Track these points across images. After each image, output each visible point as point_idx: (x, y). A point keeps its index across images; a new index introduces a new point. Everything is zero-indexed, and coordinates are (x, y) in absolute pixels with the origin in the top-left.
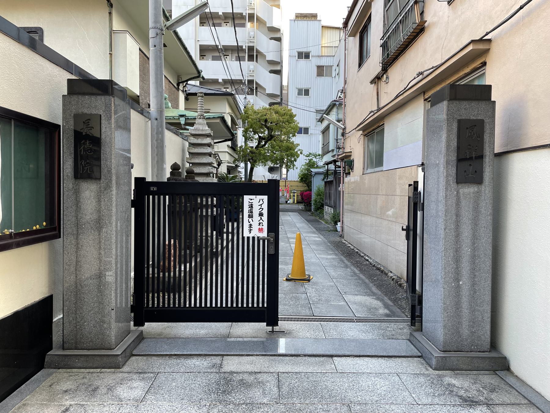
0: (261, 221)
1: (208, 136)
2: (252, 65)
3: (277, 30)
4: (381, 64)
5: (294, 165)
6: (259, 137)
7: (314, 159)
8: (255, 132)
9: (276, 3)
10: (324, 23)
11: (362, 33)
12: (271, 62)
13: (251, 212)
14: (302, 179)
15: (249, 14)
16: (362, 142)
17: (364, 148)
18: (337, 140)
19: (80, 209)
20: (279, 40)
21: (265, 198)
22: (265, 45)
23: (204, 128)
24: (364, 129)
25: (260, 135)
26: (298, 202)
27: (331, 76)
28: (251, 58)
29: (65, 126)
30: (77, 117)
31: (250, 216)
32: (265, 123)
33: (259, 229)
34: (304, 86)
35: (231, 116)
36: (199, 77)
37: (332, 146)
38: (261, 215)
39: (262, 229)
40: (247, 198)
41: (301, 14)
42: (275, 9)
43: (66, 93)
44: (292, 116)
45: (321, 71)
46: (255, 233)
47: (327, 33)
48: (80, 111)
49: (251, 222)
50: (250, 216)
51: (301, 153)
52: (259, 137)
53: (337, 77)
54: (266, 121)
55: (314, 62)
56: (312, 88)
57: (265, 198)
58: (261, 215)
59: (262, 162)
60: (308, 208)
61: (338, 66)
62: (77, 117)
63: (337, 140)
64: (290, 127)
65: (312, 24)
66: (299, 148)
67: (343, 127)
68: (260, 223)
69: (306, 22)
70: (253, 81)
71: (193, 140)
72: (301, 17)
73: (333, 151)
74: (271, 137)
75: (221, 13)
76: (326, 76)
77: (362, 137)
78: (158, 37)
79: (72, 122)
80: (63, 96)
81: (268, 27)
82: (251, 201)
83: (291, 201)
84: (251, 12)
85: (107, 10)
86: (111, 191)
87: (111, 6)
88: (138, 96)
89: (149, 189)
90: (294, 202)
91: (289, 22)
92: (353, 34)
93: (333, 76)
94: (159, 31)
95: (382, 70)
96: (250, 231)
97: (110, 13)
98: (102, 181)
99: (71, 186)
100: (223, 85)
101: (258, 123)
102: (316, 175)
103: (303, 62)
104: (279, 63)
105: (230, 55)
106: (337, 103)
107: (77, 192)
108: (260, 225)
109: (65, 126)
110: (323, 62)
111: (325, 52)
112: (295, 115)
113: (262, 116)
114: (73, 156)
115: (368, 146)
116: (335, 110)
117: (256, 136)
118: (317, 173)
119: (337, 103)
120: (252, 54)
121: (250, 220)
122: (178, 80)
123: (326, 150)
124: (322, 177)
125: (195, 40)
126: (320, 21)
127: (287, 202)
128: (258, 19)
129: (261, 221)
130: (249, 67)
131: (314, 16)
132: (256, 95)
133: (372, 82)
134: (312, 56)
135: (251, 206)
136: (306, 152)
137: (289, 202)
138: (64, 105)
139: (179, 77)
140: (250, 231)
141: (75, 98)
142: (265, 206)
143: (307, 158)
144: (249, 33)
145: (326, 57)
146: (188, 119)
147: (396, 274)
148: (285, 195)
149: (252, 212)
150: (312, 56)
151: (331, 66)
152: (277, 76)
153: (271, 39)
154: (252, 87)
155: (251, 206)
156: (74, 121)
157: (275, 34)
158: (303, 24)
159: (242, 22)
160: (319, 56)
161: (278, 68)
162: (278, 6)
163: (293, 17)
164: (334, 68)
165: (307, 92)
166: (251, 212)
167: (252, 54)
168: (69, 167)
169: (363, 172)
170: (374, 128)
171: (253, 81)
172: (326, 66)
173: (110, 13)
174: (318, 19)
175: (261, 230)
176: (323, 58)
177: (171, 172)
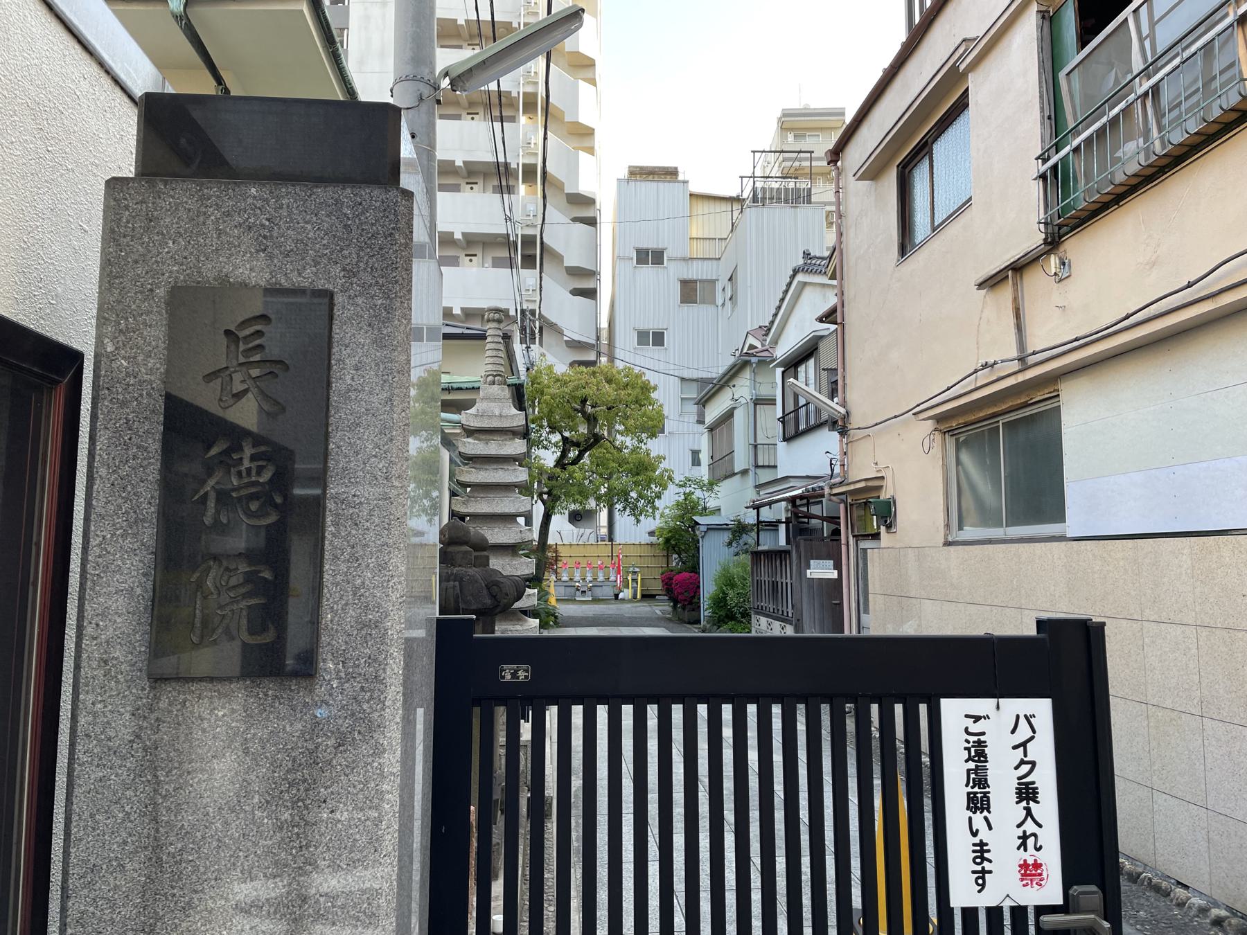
0: (1030, 827)
1: (511, 433)
2: (529, 277)
3: (589, 202)
4: (1042, 226)
5: (654, 508)
7: (698, 494)
8: (554, 428)
9: (586, 145)
10: (695, 188)
11: (904, 167)
12: (575, 272)
13: (978, 779)
14: (667, 541)
16: (937, 450)
17: (945, 467)
18: (756, 446)
19: (177, 876)
20: (592, 222)
21: (1042, 708)
22: (563, 236)
23: (505, 412)
24: (939, 419)
25: (567, 434)
26: (647, 597)
27: (713, 302)
28: (529, 261)
29: (112, 357)
30: (185, 302)
31: (978, 803)
32: (581, 406)
33: (1024, 865)
34: (652, 325)
37: (741, 460)
38: (1027, 793)
39: (1037, 865)
40: (954, 711)
41: (641, 168)
42: (583, 156)
43: (128, 169)
44: (646, 389)
45: (690, 291)
46: (1006, 889)
47: (702, 208)
48: (209, 271)
49: (984, 835)
50: (978, 803)
51: (670, 478)
52: (565, 439)
53: (728, 304)
55: (672, 272)
56: (671, 329)
57: (1042, 708)
58: (1027, 793)
60: (686, 615)
61: (730, 279)
62: (185, 302)
63: (756, 446)
64: (644, 415)
65: (665, 188)
66: (664, 465)
67: (842, 411)
68: (1024, 838)
69: (654, 185)
71: (472, 446)
72: (640, 173)
73: (744, 472)
75: (459, 163)
76: (703, 302)
77: (938, 437)
78: (424, 107)
79: (155, 334)
80: (114, 184)
82: (974, 728)
83: (627, 594)
86: (378, 751)
89: (495, 672)
90: (635, 597)
91: (615, 183)
92: (872, 173)
93: (719, 301)
94: (426, 91)
95: (1045, 242)
96: (981, 876)
98: (321, 690)
99: (123, 727)
101: (567, 406)
102: (710, 533)
103: (648, 271)
104: (593, 274)
105: (480, 255)
106: (754, 360)
107: (156, 765)
108: (1024, 845)
109: (112, 357)
110: (695, 272)
111: (699, 250)
112: (655, 388)
113: (577, 388)
114: (149, 534)
115: (958, 462)
116: (747, 374)
117: (556, 438)
118: (711, 529)
119: (754, 360)
120: (529, 252)
121: (978, 819)
123: (720, 473)
124: (727, 536)
126: (686, 182)
127: (616, 596)
129: (1030, 827)
131: (670, 174)
132: (541, 344)
133: (981, 286)
134: (670, 259)
135: (978, 753)
136: (678, 478)
137: (621, 596)
138: (112, 235)
140: (981, 876)
141: (182, 196)
142: (1044, 750)
143: (682, 490)
144: (524, 207)
145: (700, 262)
147: (1221, 899)
148: (613, 578)
149: (982, 782)
150: (670, 259)
151: (713, 282)
153: (575, 220)
154: (534, 326)
155: (978, 753)
156: (171, 327)
157: (582, 209)
158: (648, 188)
160: (684, 259)
162: (591, 151)
163: (624, 174)
164: (719, 287)
165: (659, 339)
166: (978, 779)
168: (120, 603)
169: (946, 535)
170: (995, 410)
172: (701, 281)
174: (681, 177)
175: (1030, 872)
176: (695, 262)
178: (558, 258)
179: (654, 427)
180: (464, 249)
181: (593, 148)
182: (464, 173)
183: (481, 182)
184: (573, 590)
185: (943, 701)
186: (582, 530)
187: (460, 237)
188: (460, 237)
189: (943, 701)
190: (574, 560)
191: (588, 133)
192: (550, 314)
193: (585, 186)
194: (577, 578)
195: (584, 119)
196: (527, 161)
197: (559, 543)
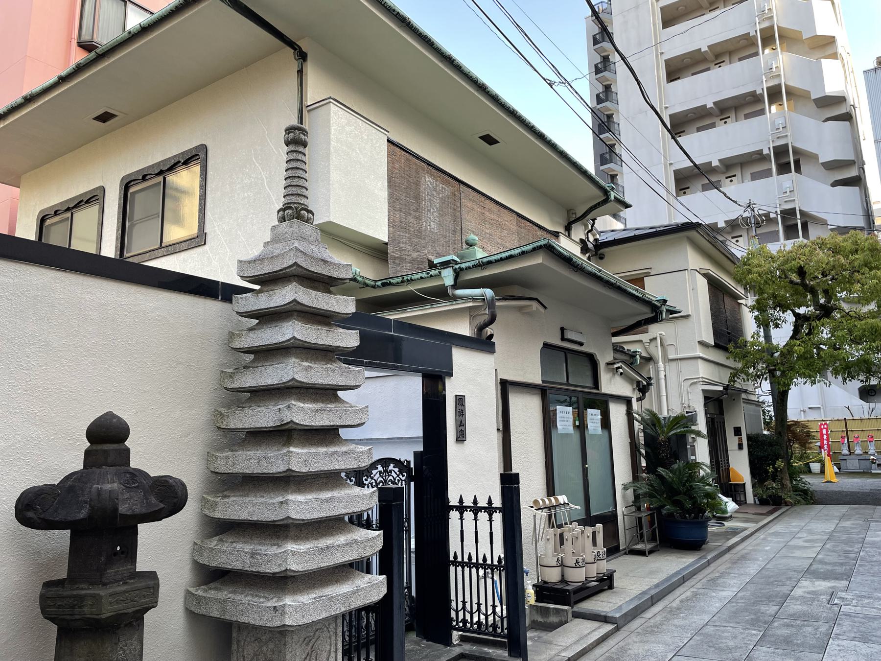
2: (788, 180)
3: (840, 100)
6: (797, 315)
8: (784, 308)
15: (768, 88)
20: (848, 117)
22: (820, 139)
28: (784, 168)
35: (706, 275)
36: (606, 201)
42: (825, 62)
54: (801, 272)
59: (804, 375)
70: (794, 209)
74: (826, 311)
75: (710, 105)
81: (815, 100)
84: (771, 83)
85: (295, 66)
87: (302, 56)
88: (386, 244)
97: (300, 72)
100: (729, 233)
104: (857, 162)
120: (787, 159)
122: (569, 217)
125: (665, 165)
128: (792, 93)
130: (780, 186)
139: (570, 211)
144: (773, 123)
146: (461, 269)
152: (854, 190)
157: (835, 108)
159: (758, 108)
161: (853, 173)
162: (834, 56)
167: (787, 159)
171: (794, 209)
173: (300, 72)
177: (87, 453)
178: (813, 157)
179: (589, 259)
180: (723, 173)
181: (836, 53)
182: (717, 111)
183: (733, 115)
184: (868, 463)
185: (140, 526)
186: (872, 405)
187: (717, 164)
188: (717, 164)
189: (140, 526)
190: (867, 433)
191: (830, 41)
192: (812, 209)
193: (832, 86)
194: (872, 451)
195: (823, 29)
196: (771, 84)
197: (849, 417)
